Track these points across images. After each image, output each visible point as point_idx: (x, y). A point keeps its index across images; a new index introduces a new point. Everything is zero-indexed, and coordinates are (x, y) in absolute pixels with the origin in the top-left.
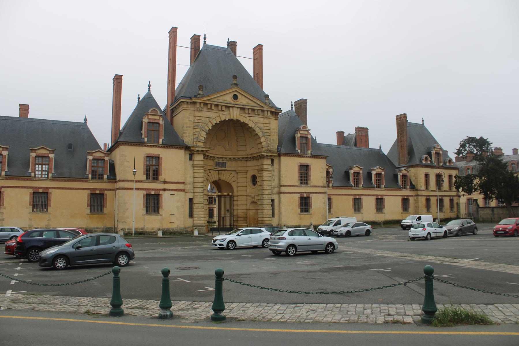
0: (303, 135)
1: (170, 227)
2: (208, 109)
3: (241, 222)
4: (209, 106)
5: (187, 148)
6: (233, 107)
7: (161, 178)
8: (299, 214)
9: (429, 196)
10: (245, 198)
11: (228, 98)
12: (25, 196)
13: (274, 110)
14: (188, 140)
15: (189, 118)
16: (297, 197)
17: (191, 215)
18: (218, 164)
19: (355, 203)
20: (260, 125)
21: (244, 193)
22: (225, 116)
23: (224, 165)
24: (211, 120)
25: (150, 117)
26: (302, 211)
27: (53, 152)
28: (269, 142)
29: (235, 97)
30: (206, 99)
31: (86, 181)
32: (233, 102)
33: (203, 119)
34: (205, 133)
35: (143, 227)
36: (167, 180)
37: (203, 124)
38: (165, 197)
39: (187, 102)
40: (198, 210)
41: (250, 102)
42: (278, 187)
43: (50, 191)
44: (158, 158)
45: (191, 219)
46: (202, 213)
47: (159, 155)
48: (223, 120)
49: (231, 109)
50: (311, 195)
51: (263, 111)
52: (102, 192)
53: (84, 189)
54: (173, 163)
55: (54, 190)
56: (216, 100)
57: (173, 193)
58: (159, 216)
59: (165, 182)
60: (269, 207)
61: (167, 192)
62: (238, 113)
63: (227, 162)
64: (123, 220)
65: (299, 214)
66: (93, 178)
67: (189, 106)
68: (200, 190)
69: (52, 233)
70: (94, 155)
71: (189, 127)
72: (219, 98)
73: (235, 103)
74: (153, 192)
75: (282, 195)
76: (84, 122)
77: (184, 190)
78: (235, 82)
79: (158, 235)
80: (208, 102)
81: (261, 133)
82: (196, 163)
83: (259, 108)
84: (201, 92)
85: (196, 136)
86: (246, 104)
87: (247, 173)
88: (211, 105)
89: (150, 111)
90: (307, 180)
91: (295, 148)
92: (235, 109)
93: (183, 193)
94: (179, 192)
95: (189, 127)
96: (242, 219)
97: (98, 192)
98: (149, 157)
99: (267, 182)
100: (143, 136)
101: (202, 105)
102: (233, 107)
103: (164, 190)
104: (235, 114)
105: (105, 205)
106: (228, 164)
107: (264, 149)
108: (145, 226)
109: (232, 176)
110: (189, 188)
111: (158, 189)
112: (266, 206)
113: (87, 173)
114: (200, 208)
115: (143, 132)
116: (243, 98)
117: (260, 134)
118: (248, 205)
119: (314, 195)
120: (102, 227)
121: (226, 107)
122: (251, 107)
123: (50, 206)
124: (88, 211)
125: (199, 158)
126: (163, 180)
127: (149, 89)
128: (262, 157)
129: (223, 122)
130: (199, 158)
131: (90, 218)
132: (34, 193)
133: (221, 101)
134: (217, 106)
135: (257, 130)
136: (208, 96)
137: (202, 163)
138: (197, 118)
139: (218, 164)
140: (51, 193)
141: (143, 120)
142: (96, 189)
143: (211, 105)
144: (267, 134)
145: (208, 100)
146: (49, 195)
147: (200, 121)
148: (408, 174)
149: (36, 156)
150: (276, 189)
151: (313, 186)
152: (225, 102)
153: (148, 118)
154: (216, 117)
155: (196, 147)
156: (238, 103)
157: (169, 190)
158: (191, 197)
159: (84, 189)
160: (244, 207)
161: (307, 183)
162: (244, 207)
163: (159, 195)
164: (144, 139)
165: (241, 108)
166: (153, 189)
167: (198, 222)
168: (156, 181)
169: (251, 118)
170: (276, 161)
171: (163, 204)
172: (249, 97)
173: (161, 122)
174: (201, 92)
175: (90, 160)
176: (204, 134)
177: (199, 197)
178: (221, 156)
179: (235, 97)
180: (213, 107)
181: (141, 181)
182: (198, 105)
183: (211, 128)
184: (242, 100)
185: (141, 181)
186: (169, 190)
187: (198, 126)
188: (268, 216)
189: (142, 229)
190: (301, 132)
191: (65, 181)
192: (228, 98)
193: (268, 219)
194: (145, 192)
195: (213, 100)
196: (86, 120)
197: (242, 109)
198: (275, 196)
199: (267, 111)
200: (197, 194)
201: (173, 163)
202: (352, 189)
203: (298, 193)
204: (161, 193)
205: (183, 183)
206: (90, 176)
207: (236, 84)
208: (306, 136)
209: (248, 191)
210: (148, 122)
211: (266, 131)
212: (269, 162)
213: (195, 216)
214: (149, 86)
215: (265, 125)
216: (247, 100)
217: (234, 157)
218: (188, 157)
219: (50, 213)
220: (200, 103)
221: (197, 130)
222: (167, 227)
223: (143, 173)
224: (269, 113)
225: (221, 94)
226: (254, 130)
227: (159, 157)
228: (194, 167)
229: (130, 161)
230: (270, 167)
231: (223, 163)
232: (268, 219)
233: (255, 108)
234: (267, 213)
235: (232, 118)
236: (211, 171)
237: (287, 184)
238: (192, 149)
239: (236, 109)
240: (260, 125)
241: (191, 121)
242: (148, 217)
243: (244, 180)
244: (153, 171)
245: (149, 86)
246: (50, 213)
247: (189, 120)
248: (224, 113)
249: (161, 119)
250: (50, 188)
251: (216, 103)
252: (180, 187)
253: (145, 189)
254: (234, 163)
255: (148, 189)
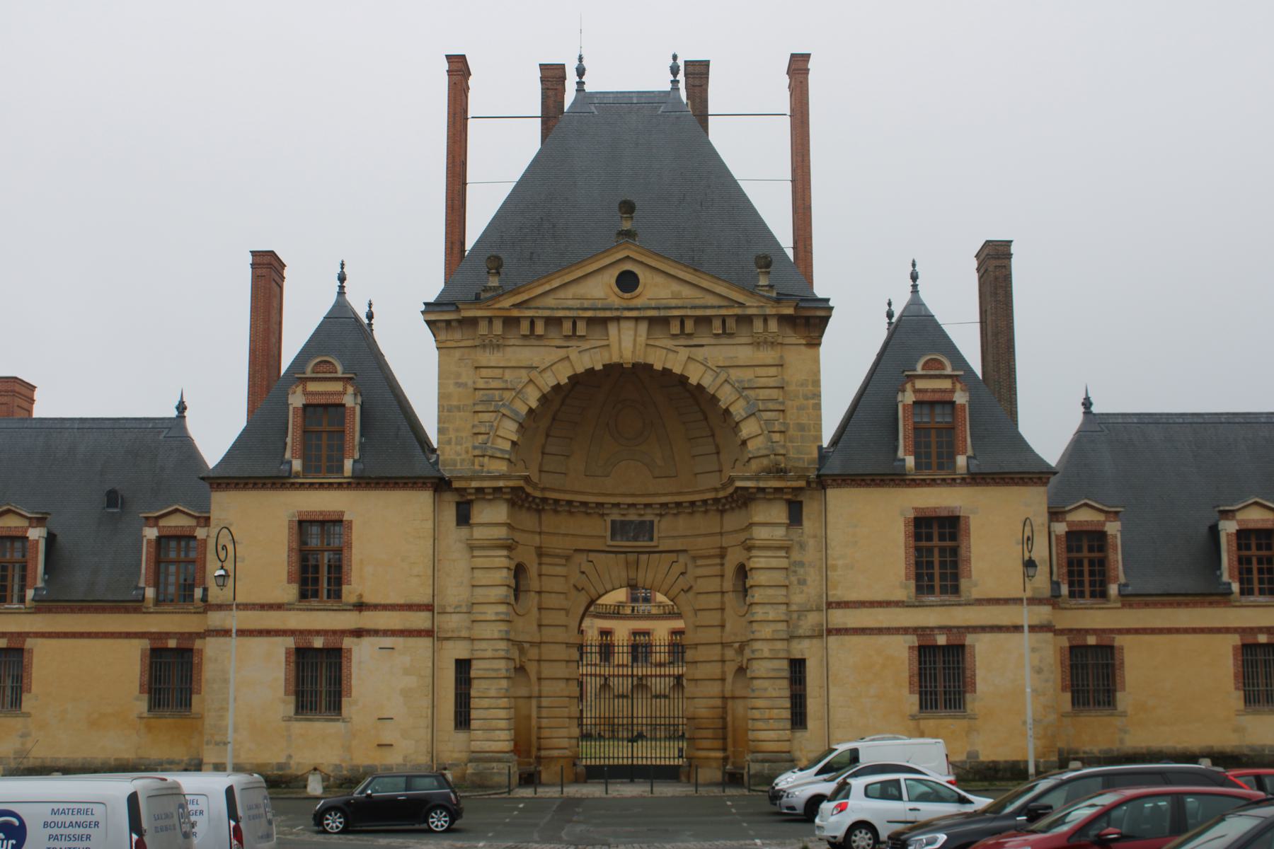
0: (927, 397)
1: (377, 763)
2: (717, 335)
3: (707, 744)
4: (525, 328)
5: (440, 485)
6: (618, 319)
7: (350, 593)
8: (913, 717)
9: (23, 635)
10: (715, 652)
11: (599, 289)
12: (122, 664)
13: (790, 311)
14: (455, 458)
15: (459, 375)
16: (901, 649)
17: (463, 720)
18: (619, 529)
19: (1245, 663)
20: (735, 374)
21: (713, 635)
22: (587, 357)
23: (645, 529)
24: (534, 374)
25: (312, 387)
26: (923, 706)
27: (40, 521)
28: (776, 437)
29: (627, 282)
30: (507, 303)
31: (137, 610)
32: (616, 302)
33: (508, 375)
34: (512, 426)
35: (283, 760)
36: (369, 598)
37: (508, 395)
38: (364, 659)
39: (448, 322)
40: (485, 703)
41: (687, 291)
42: (819, 609)
43: (29, 643)
44: (332, 524)
45: (462, 736)
46: (503, 714)
47: (342, 513)
48: (580, 370)
49: (613, 329)
50: (970, 639)
51: (745, 320)
52: (185, 645)
53: (128, 635)
54: (391, 538)
55: (40, 641)
56: (550, 301)
57: (388, 641)
58: (340, 725)
59: (360, 606)
60: (781, 690)
61: (366, 641)
62: (642, 338)
63: (656, 520)
64: (217, 738)
65: (913, 717)
66: (1072, 594)
67: (458, 335)
68: (495, 631)
69: (1100, 779)
70: (162, 523)
71: (458, 408)
72: (561, 294)
73: (624, 304)
74: (318, 643)
75: (832, 639)
76: (174, 414)
77: (429, 633)
78: (627, 225)
79: (309, 789)
80: (515, 313)
81: (742, 403)
82: (478, 533)
83: (723, 312)
84: (494, 282)
85: (481, 438)
86: (674, 303)
87: (722, 556)
88: (724, 322)
89: (919, 366)
90: (956, 577)
91: (896, 449)
92: (627, 327)
93: (425, 642)
94: (411, 641)
95: (458, 408)
96: (709, 733)
97: (172, 643)
98: (303, 525)
99: (770, 592)
100: (288, 455)
101: (498, 328)
102: (618, 319)
103: (359, 633)
104: (626, 344)
105: (195, 686)
106: (664, 527)
107: (754, 465)
108: (290, 757)
109: (677, 569)
110: (453, 622)
111: (334, 632)
112: (766, 683)
113: (1226, 578)
114: (493, 693)
115: (289, 440)
116: (659, 279)
117: (738, 410)
118: (730, 678)
119: (986, 637)
120: (186, 758)
121: (591, 321)
122: (689, 312)
123: (29, 691)
124: (142, 705)
125: (492, 516)
126: (353, 599)
127: (915, 286)
128: (743, 499)
129: (582, 382)
130: (492, 516)
131: (149, 729)
132: (1072, 648)
133: (570, 303)
134: (553, 322)
135: (726, 396)
136: (515, 292)
137: (502, 533)
138: (484, 372)
139: (619, 529)
140: (31, 651)
141: (900, 398)
142: (168, 635)
143: (724, 322)
144: (771, 406)
145: (515, 306)
146: (26, 655)
147: (494, 384)
148: (200, 533)
149: (159, 539)
150: (812, 619)
151: (980, 602)
152: (586, 304)
153: (305, 393)
154: (555, 363)
155: (472, 479)
156: (638, 302)
157: (375, 633)
158: (464, 655)
159: (128, 635)
160: (715, 689)
161: (956, 590)
162: (715, 689)
163: (1111, 648)
164: (290, 463)
165: (652, 321)
166: (318, 633)
167: (487, 746)
168: (953, 598)
169: (700, 353)
170: (810, 510)
171: (354, 682)
172: (681, 274)
173: (349, 400)
174: (494, 282)
175: (149, 541)
176: (509, 429)
177: (489, 654)
178: (630, 500)
179: (627, 282)
180: (540, 329)
181: (279, 607)
182: (483, 329)
183: (534, 405)
184: (656, 290)
185: (279, 607)
186: (375, 633)
187: (489, 401)
188: (772, 724)
189: (280, 766)
190: (920, 384)
191: (72, 611)
192: (599, 289)
193: (772, 735)
194: (290, 642)
195: (533, 304)
196: (181, 407)
197: (658, 322)
198: (806, 644)
199: (765, 319)
200: (484, 645)
201: (391, 538)
202: (1228, 604)
203: (905, 631)
204: (347, 642)
205: (429, 608)
206: (1235, 587)
207: (629, 234)
208: (946, 397)
209: (728, 626)
210: (305, 406)
211: (764, 394)
212: (778, 513)
213: (474, 724)
214: (914, 277)
215: (760, 371)
216: (676, 287)
217: (678, 499)
218: (450, 514)
219: (28, 715)
220: (490, 319)
221: (486, 417)
222: (367, 762)
223: (285, 576)
224: (773, 326)
225: (567, 279)
226: (714, 399)
227: (301, 522)
228: (472, 548)
229: (254, 538)
230: (780, 532)
231: (643, 523)
232: (772, 735)
233: (709, 312)
234: (767, 714)
235: (615, 359)
236: (592, 556)
237: (853, 596)
238: (456, 485)
239: (631, 324)
240: (735, 374)
241: (465, 385)
242: (299, 727)
243: (714, 584)
244: (319, 565)
245: (914, 277)
246: (28, 715)
247: (458, 385)
248: (586, 345)
249: (350, 390)
250: (28, 635)
251: (547, 313)
252: (425, 620)
253: (292, 633)
254: (682, 524)
255: (301, 632)
